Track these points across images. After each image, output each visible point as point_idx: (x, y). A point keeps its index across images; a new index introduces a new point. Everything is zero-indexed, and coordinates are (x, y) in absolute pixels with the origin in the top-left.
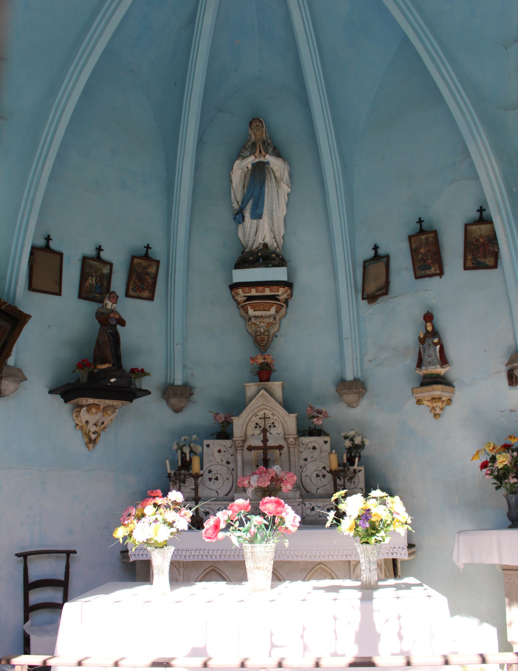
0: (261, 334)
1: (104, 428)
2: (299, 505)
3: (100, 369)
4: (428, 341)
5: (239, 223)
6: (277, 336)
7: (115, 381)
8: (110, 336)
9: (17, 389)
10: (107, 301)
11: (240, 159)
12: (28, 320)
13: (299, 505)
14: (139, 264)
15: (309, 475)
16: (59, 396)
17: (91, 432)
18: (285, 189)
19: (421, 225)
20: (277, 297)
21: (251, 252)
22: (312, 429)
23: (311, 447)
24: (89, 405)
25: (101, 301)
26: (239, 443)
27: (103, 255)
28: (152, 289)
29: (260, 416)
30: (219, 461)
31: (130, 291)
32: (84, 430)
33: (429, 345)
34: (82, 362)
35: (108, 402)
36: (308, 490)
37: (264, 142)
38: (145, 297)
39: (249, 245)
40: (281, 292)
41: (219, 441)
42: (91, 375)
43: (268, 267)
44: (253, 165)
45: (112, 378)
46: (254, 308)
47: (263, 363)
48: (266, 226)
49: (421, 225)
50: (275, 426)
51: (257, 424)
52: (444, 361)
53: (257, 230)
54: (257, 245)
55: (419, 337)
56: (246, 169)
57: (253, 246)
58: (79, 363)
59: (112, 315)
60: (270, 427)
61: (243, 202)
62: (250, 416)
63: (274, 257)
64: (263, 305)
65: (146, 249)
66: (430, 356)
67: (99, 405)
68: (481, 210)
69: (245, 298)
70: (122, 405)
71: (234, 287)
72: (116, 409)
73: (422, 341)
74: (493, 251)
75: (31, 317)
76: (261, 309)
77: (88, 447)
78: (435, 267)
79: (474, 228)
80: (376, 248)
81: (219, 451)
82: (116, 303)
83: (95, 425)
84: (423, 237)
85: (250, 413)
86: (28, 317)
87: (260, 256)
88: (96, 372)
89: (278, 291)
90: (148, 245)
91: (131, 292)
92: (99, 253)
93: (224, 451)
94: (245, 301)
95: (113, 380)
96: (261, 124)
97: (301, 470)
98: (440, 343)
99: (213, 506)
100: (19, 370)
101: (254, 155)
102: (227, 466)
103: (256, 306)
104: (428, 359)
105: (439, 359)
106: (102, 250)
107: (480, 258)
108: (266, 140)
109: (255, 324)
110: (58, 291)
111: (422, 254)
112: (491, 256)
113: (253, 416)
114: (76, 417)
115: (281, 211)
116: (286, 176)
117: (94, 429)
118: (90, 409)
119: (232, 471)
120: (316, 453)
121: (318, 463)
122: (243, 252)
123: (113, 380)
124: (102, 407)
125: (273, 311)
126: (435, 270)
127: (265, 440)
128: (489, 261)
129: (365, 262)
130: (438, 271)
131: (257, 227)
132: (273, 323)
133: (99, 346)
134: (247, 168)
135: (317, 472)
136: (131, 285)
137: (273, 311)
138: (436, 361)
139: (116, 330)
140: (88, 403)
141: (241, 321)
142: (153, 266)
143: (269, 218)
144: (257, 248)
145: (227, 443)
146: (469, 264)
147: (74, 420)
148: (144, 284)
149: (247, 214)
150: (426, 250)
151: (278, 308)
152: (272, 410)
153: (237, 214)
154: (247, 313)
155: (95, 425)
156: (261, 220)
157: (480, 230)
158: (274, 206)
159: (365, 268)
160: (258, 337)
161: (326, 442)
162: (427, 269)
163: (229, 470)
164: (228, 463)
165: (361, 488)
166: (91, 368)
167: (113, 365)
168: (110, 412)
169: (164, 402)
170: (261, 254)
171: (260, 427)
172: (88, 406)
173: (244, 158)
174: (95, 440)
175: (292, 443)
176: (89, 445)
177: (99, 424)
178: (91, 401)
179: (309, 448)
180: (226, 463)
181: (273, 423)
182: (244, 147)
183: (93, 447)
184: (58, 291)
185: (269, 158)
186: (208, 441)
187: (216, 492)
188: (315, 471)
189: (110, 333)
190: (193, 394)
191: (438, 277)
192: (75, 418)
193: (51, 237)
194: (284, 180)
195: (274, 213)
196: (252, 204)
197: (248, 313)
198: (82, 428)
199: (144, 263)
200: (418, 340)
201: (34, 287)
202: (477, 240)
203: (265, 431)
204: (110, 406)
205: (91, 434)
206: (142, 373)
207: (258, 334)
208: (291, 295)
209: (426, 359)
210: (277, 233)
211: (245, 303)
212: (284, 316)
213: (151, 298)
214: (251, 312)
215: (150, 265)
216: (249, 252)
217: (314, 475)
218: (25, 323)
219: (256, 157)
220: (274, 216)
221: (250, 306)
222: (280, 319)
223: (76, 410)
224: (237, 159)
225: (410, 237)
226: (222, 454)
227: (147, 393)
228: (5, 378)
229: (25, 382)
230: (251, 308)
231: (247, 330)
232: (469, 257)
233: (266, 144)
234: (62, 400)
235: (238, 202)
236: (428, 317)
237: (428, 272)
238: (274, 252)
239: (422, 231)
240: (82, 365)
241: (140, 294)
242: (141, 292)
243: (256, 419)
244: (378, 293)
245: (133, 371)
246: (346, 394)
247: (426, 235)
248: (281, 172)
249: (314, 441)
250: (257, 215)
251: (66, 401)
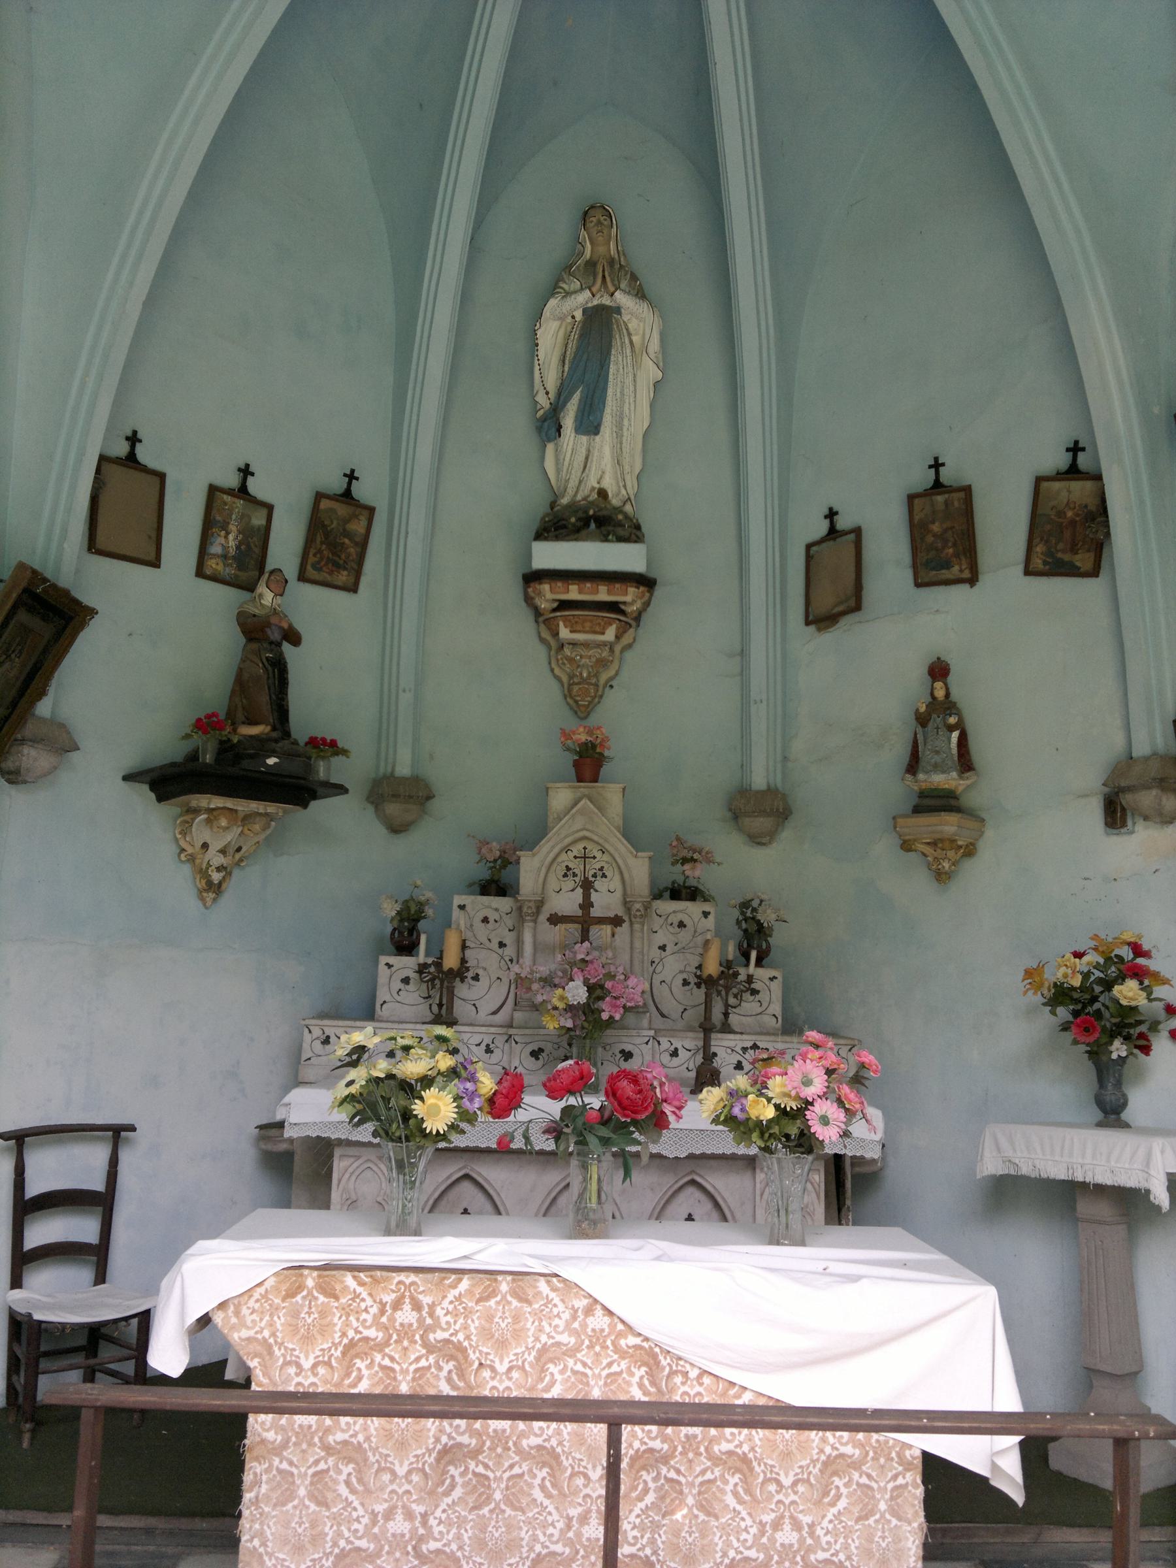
0: (583, 681)
1: (241, 860)
2: (647, 1043)
3: (245, 736)
4: (935, 720)
5: (549, 441)
6: (611, 687)
7: (275, 763)
8: (266, 663)
9: (55, 768)
10: (262, 588)
11: (559, 297)
12: (91, 619)
13: (647, 1043)
14: (332, 510)
15: (668, 980)
16: (145, 788)
17: (213, 867)
18: (650, 372)
19: (937, 473)
20: (623, 607)
21: (573, 507)
22: (679, 885)
23: (676, 923)
24: (213, 809)
25: (250, 588)
26: (530, 907)
27: (253, 486)
28: (356, 567)
29: (575, 853)
30: (484, 940)
31: (309, 567)
32: (198, 861)
33: (937, 728)
34: (205, 718)
35: (254, 806)
36: (665, 1012)
37: (611, 262)
38: (340, 584)
39: (570, 491)
40: (630, 596)
41: (485, 899)
42: (225, 748)
43: (606, 540)
44: (585, 311)
45: (269, 757)
46: (572, 627)
47: (586, 744)
48: (607, 451)
49: (937, 473)
50: (604, 876)
51: (568, 868)
52: (965, 762)
53: (587, 458)
54: (586, 492)
55: (917, 710)
56: (569, 319)
57: (577, 492)
58: (199, 720)
59: (274, 620)
60: (595, 876)
61: (559, 394)
62: (556, 850)
63: (620, 521)
64: (591, 621)
65: (347, 479)
66: (937, 752)
67: (236, 811)
68: (1075, 449)
69: (555, 605)
70: (285, 812)
71: (533, 578)
72: (272, 820)
73: (922, 720)
74: (1092, 539)
75: (97, 613)
76: (587, 629)
77: (203, 899)
78: (961, 565)
79: (1057, 485)
80: (831, 514)
81: (485, 920)
82: (281, 595)
83: (223, 851)
84: (940, 499)
85: (557, 844)
86: (92, 612)
87: (591, 517)
88: (235, 741)
89: (626, 594)
90: (353, 471)
91: (311, 572)
92: (244, 480)
93: (496, 921)
94: (554, 610)
95: (271, 761)
96: (609, 219)
97: (651, 969)
98: (961, 727)
99: (469, 1035)
100: (62, 726)
101: (590, 290)
102: (500, 951)
103: (576, 622)
104: (932, 758)
105: (956, 759)
106: (252, 474)
107: (1064, 551)
108: (616, 256)
109: (571, 660)
110: (152, 557)
111: (935, 535)
112: (1088, 551)
113: (561, 851)
114: (180, 833)
115: (639, 417)
116: (655, 345)
117: (219, 860)
118: (216, 818)
119: (509, 963)
120: (684, 936)
121: (688, 956)
122: (553, 505)
123: (271, 761)
124: (241, 815)
125: (610, 634)
126: (961, 571)
127: (587, 905)
128: (1083, 560)
129: (809, 547)
130: (967, 574)
131: (589, 451)
132: (608, 661)
133: (241, 685)
134: (573, 317)
135: (685, 976)
136: (311, 555)
137: (610, 634)
138: (950, 763)
139: (281, 654)
140: (212, 806)
141: (541, 652)
142: (362, 518)
143: (615, 434)
144: (585, 499)
145: (504, 904)
146: (1037, 563)
147: (177, 840)
148: (339, 557)
149: (568, 421)
150: (945, 526)
151: (621, 630)
152: (601, 841)
153: (544, 419)
154: (556, 634)
155: (223, 851)
156: (598, 438)
157: (1069, 492)
158: (626, 406)
159: (809, 558)
160: (576, 688)
161: (706, 914)
162: (942, 568)
163: (502, 961)
164: (502, 945)
165: (774, 1015)
166: (224, 733)
167: (274, 729)
168: (257, 827)
169: (371, 809)
170: (595, 512)
171: (575, 875)
172: (210, 811)
173: (568, 294)
174: (220, 884)
175: (638, 913)
176: (205, 894)
177: (231, 850)
178: (218, 802)
179: (672, 924)
180: (497, 945)
181: (601, 869)
182: (567, 268)
183: (214, 900)
184: (152, 557)
185: (622, 299)
186: (464, 897)
187: (474, 1005)
188: (681, 972)
189: (267, 658)
190: (434, 796)
191: (967, 586)
192: (179, 836)
193: (139, 436)
194: (651, 350)
195: (626, 422)
196: (580, 400)
197: (558, 634)
198: (192, 859)
199: (342, 510)
200: (914, 717)
201: (101, 541)
202: (1061, 514)
203: (587, 886)
204: (260, 814)
205: (212, 871)
206: (331, 747)
207: (576, 680)
208: (647, 604)
209: (926, 755)
210: (627, 468)
211: (552, 615)
212: (630, 646)
213: (353, 588)
214: (564, 633)
215: (355, 516)
216: (569, 506)
217: (678, 981)
218: (82, 625)
219: (594, 296)
220: (625, 429)
221: (564, 622)
222: (622, 651)
223: (182, 819)
224: (552, 294)
225: (911, 498)
226: (491, 925)
227: (341, 789)
228: (30, 743)
229: (74, 756)
230: (566, 627)
231: (552, 670)
232: (1039, 549)
233: (617, 266)
234: (153, 796)
235: (547, 393)
236: (939, 671)
237: (945, 574)
238: (619, 510)
239: (937, 485)
240: (202, 726)
241: (329, 578)
242: (331, 573)
243: (567, 859)
244: (840, 608)
245: (313, 742)
246: (750, 816)
247: (946, 496)
248: (644, 334)
249: (681, 911)
250: (589, 425)
251: (160, 799)
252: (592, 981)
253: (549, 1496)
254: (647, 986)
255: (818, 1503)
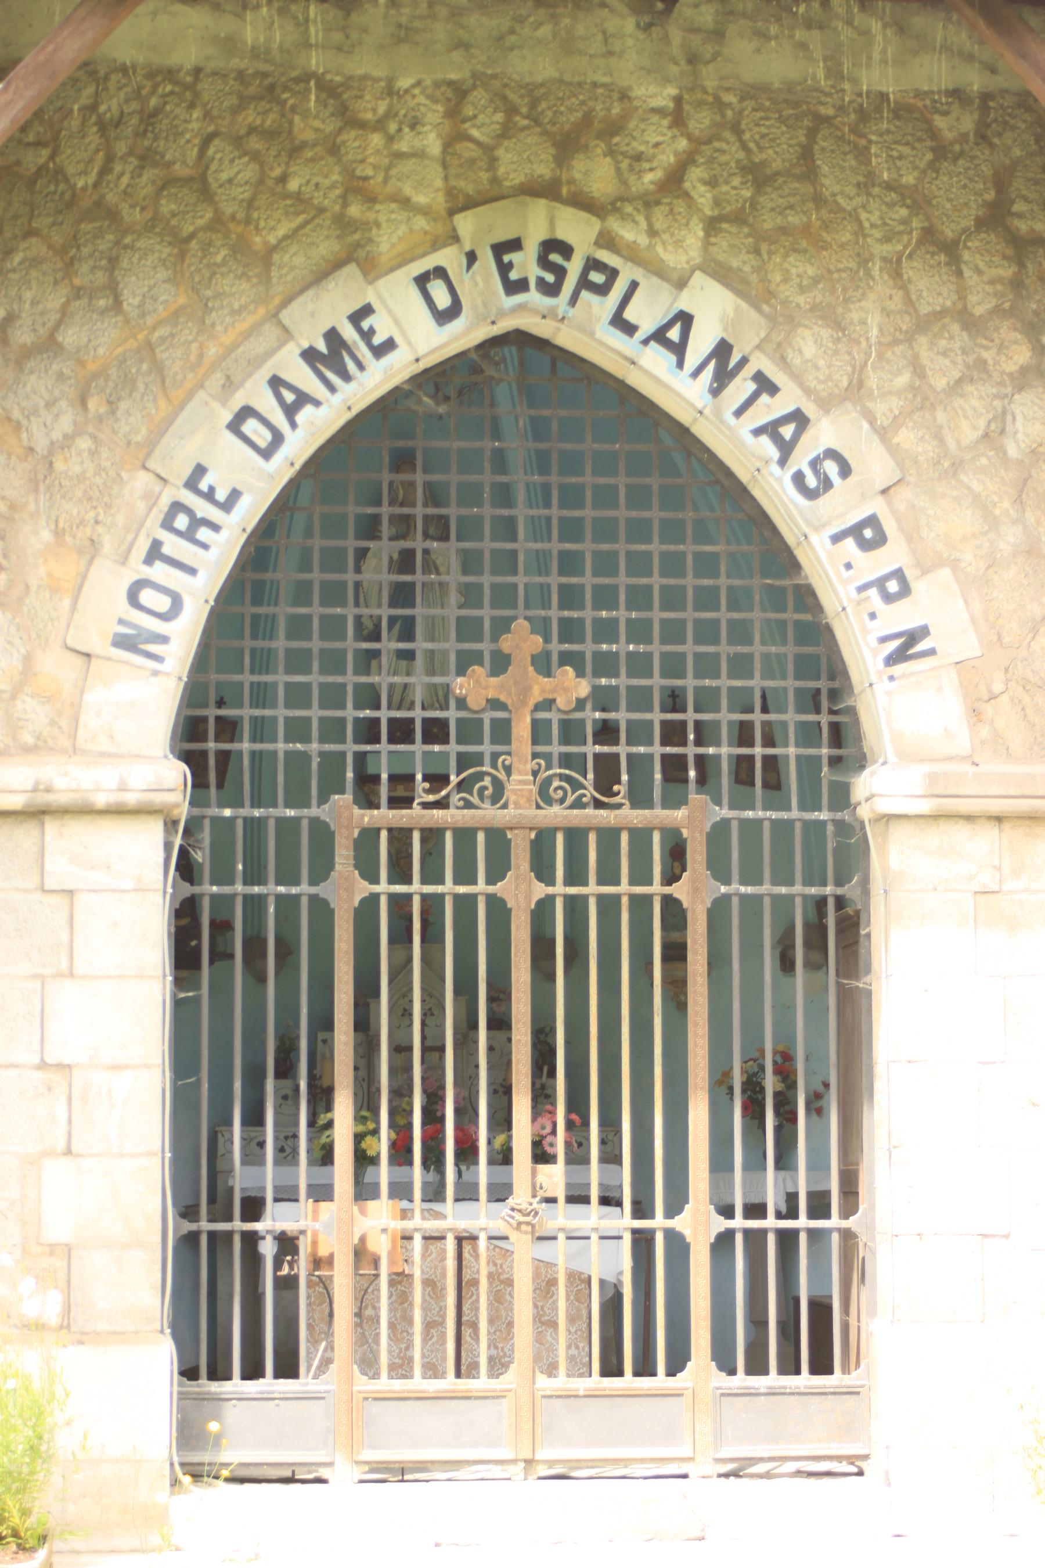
6: (431, 854)
45: (192, 940)
181: (430, 1009)
252: (429, 1091)
253: (432, 1298)
254: (466, 1093)
255: (545, 1297)
